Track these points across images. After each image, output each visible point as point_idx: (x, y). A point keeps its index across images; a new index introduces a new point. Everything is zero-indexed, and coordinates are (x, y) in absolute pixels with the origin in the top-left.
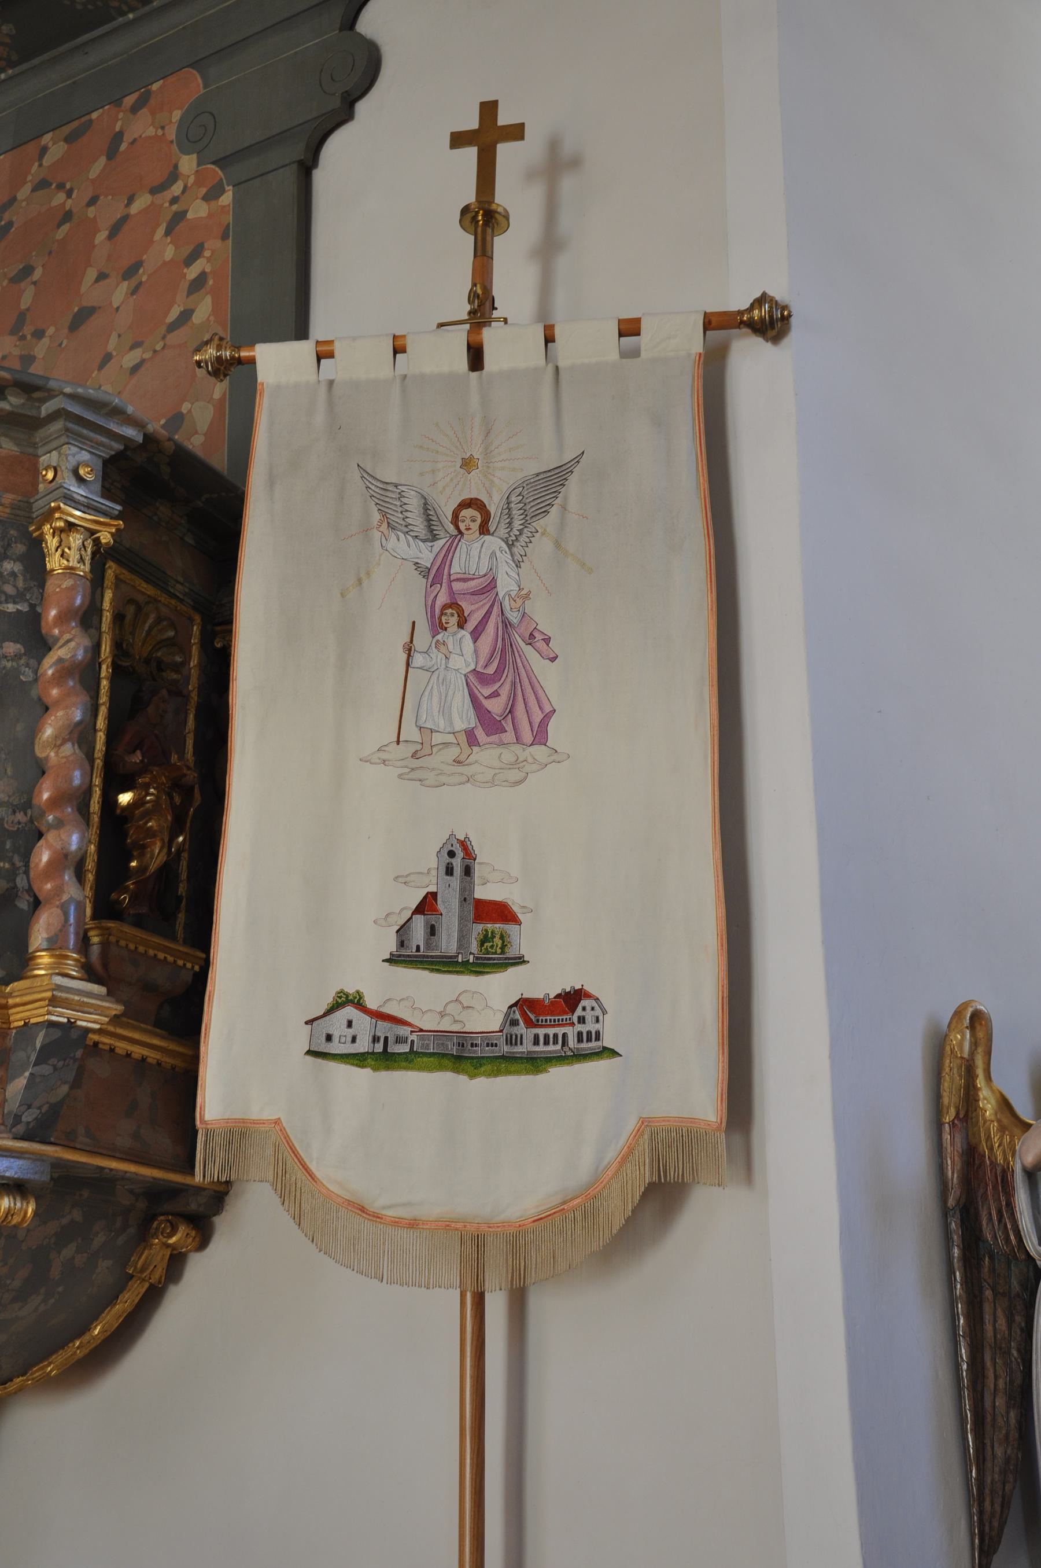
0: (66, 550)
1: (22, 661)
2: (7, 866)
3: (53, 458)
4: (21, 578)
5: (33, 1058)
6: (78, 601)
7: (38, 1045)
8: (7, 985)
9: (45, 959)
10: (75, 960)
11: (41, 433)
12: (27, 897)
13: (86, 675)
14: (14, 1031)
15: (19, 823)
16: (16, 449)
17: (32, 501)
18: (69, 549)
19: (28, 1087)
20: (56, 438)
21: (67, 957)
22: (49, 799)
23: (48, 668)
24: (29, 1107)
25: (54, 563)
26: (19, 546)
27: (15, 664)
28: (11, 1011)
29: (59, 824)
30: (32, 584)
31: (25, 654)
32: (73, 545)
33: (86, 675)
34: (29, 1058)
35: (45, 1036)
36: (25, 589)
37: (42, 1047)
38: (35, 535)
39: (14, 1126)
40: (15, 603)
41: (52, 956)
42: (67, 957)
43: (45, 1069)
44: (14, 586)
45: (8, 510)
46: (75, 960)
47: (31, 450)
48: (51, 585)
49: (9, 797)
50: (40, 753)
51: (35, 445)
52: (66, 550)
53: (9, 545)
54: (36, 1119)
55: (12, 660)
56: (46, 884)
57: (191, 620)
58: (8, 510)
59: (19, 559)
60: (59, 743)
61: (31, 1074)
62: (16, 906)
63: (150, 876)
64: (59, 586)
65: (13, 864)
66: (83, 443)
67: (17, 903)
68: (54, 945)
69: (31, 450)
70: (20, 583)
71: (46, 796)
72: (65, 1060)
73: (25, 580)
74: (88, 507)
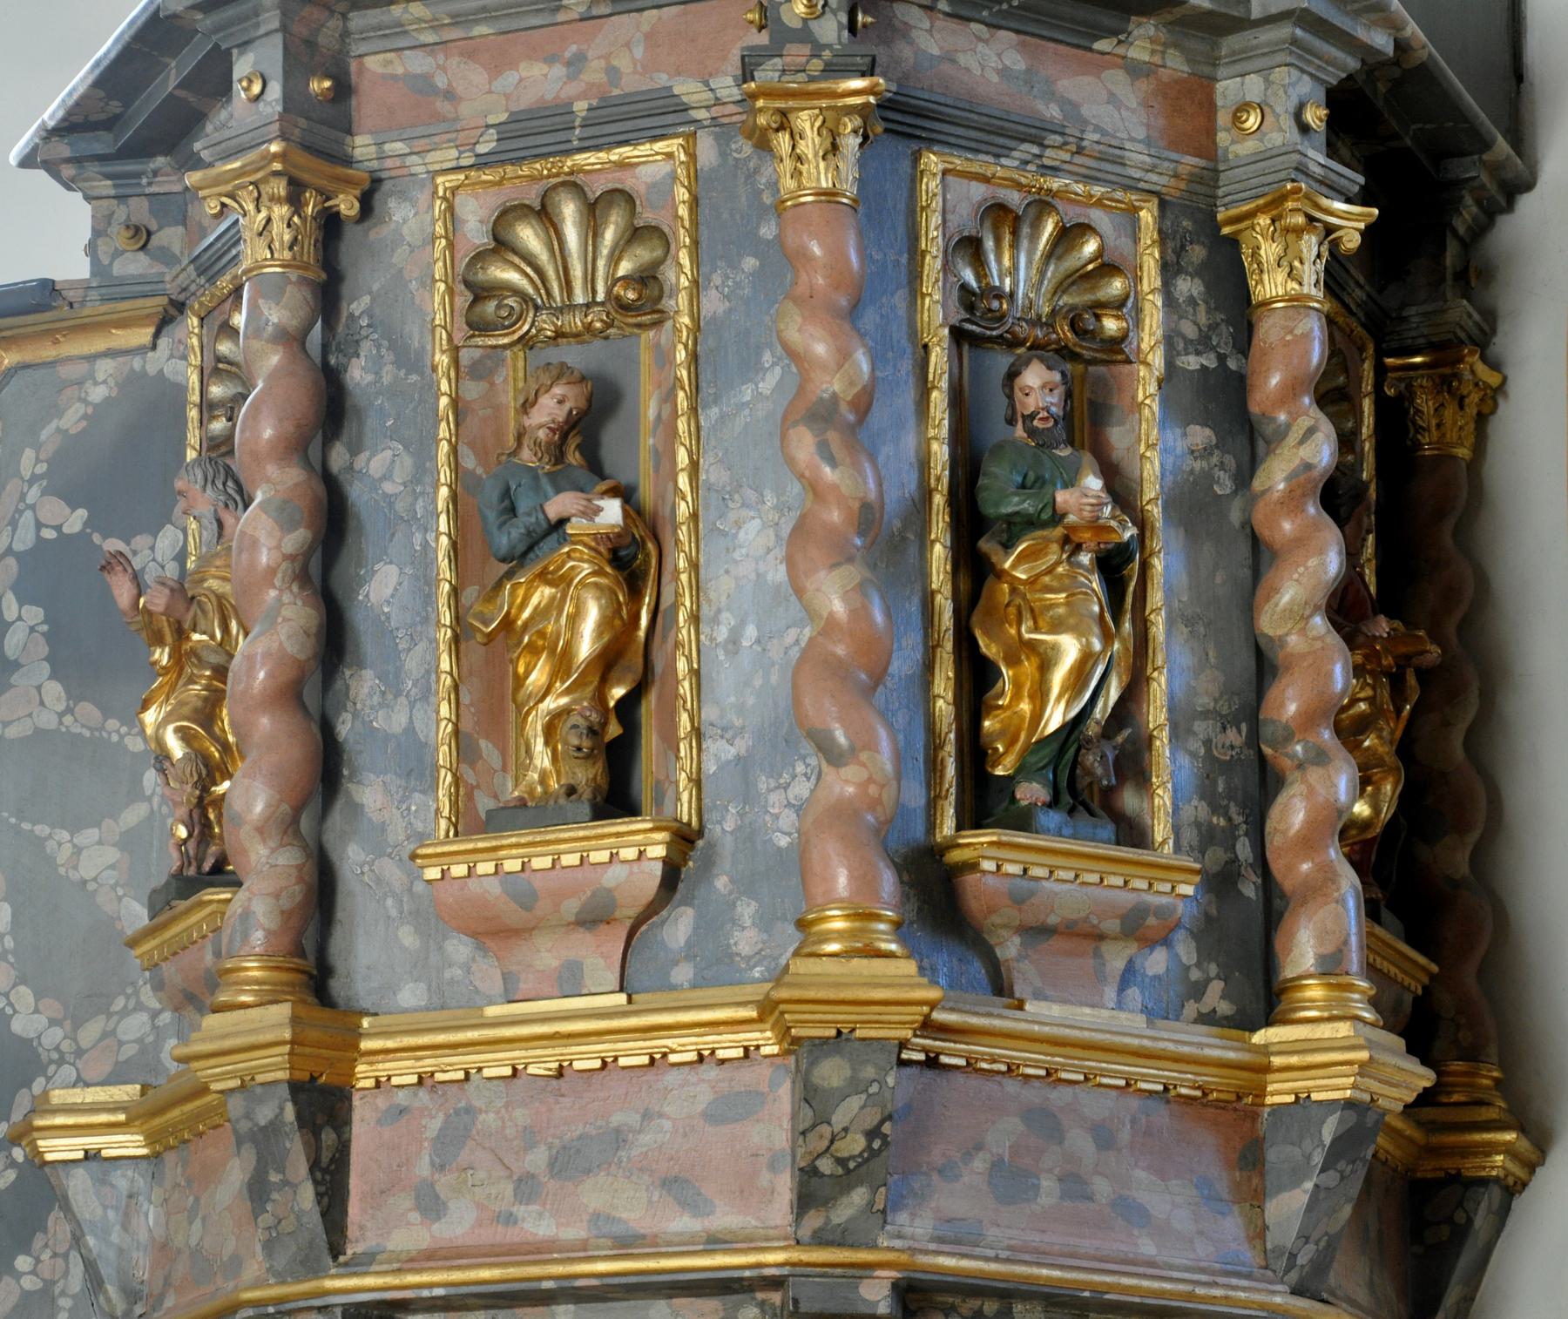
0: (1297, 263)
1: (1215, 460)
2: (1222, 822)
3: (1253, 87)
4: (1202, 308)
5: (1318, 1158)
6: (1315, 359)
7: (1327, 1138)
8: (1253, 1030)
9: (1314, 991)
10: (1362, 992)
11: (1231, 43)
12: (1254, 878)
13: (1336, 496)
14: (1267, 1110)
15: (1232, 747)
16: (1186, 69)
17: (1221, 168)
18: (1302, 263)
19: (1311, 1207)
20: (1263, 54)
21: (1350, 987)
22: (1299, 713)
23: (1276, 476)
24: (1307, 1240)
25: (1271, 285)
26: (1197, 248)
27: (1205, 464)
28: (1270, 1077)
29: (1320, 757)
30: (1220, 316)
31: (1217, 446)
32: (1305, 254)
33: (1336, 496)
34: (1309, 1158)
35: (1341, 1121)
36: (1209, 327)
37: (1334, 1142)
38: (1226, 230)
39: (1286, 1272)
40: (1198, 353)
41: (1329, 986)
42: (1350, 987)
43: (1331, 1178)
44: (1195, 323)
45: (1183, 185)
46: (1362, 992)
47: (1207, 70)
48: (1269, 330)
49: (1216, 701)
50: (1268, 623)
51: (1214, 63)
52: (1297, 263)
53: (1183, 247)
54: (1311, 1261)
55: (1202, 457)
56: (1304, 861)
57: (1361, 349)
58: (1183, 185)
59: (1199, 272)
60: (1307, 612)
61: (1316, 1186)
62: (1239, 893)
63: (1374, 838)
64: (1291, 332)
65: (1230, 820)
66: (1309, 62)
67: (1240, 886)
68: (1330, 967)
69: (1207, 70)
70: (1203, 318)
71: (1292, 708)
72: (1354, 1162)
73: (1208, 312)
74: (1321, 182)
